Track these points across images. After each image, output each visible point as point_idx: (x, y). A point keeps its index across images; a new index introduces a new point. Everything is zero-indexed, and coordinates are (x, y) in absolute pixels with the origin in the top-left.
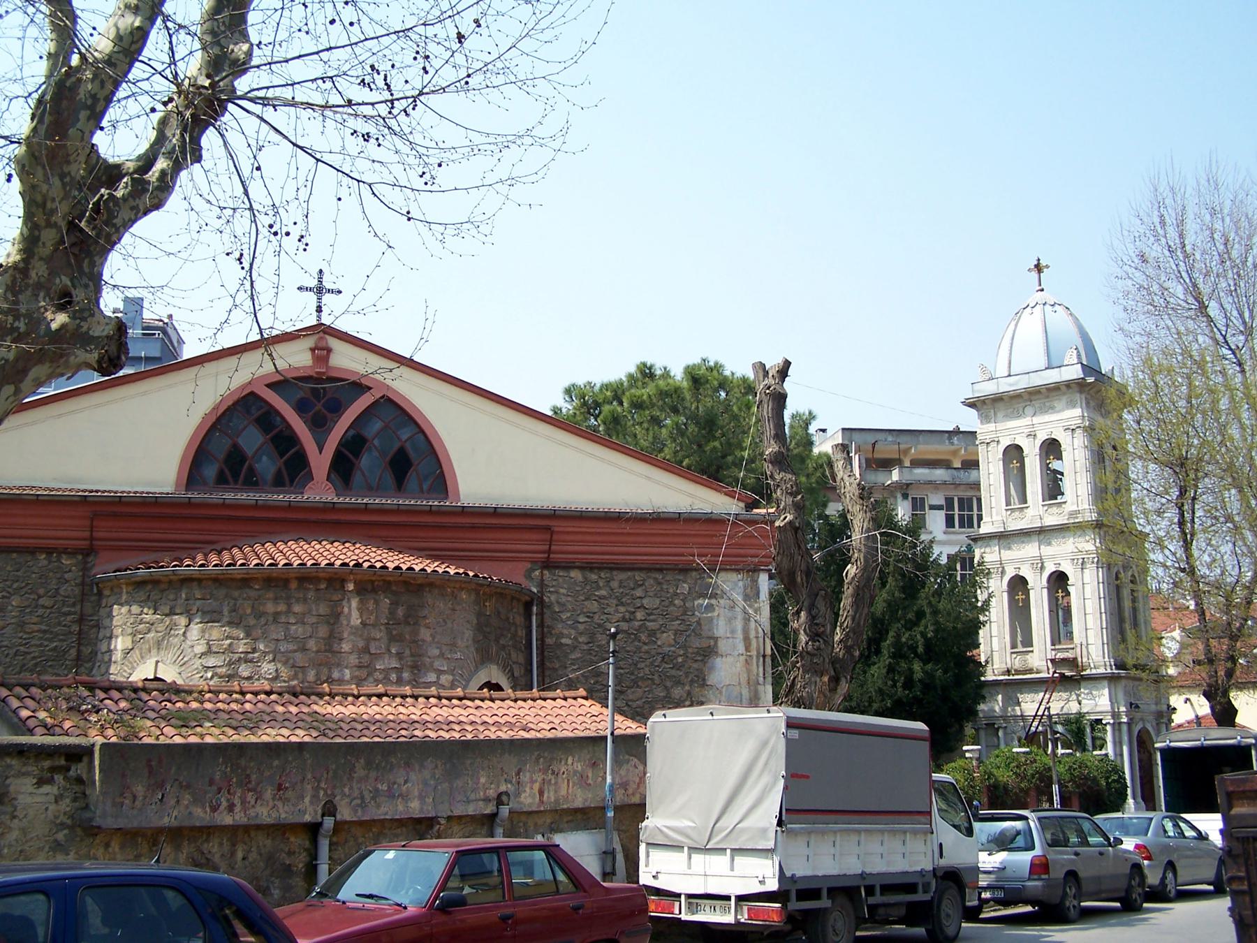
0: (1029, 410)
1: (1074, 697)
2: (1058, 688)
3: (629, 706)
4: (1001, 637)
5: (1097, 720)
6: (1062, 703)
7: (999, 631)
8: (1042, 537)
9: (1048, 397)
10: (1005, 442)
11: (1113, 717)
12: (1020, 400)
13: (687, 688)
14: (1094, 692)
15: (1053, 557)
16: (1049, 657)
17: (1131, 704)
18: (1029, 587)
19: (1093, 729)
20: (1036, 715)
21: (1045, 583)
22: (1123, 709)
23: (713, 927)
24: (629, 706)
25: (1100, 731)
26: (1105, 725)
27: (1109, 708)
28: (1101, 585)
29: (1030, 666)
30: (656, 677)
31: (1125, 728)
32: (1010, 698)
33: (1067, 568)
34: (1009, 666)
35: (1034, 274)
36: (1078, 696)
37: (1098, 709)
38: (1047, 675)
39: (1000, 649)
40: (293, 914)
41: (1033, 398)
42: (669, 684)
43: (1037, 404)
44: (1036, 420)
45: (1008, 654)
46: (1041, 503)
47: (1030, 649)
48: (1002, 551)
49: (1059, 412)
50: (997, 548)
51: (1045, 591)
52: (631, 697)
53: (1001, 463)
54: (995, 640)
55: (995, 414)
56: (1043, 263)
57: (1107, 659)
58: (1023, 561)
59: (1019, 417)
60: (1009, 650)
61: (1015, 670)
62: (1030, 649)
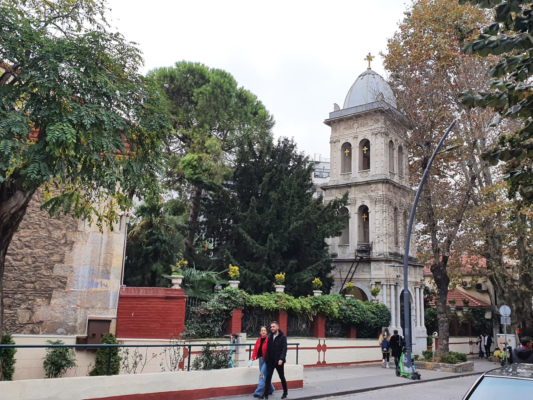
0: (356, 125)
3: (20, 240)
10: (343, 142)
12: (351, 121)
13: (64, 232)
18: (352, 147)
24: (20, 240)
30: (42, 223)
33: (367, 203)
35: (367, 62)
40: (316, 293)
42: (51, 228)
43: (360, 122)
52: (22, 234)
55: (340, 128)
56: (372, 55)
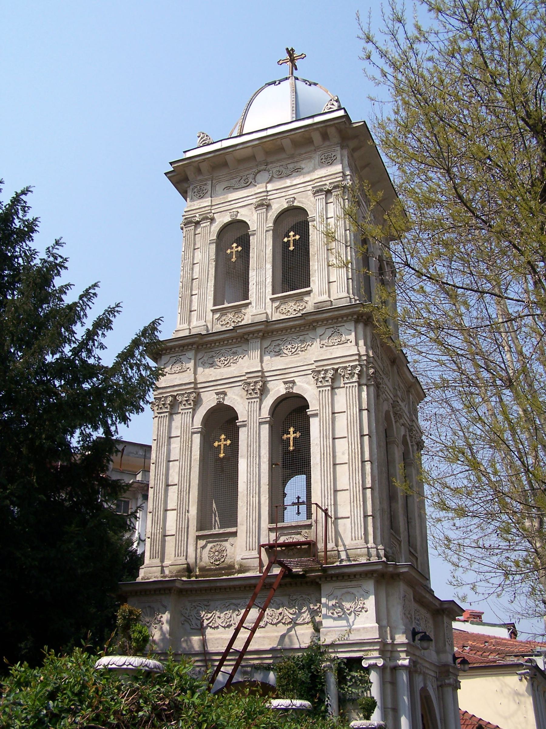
1: (306, 616)
2: (277, 599)
4: (181, 510)
5: (349, 659)
6: (282, 629)
7: (180, 499)
8: (266, 343)
9: (292, 156)
10: (223, 219)
11: (383, 653)
14: (347, 605)
15: (284, 371)
16: (264, 541)
17: (414, 633)
19: (341, 680)
20: (227, 652)
21: (265, 413)
22: (401, 638)
23: (151, 356)
25: (355, 685)
26: (367, 670)
27: (375, 635)
28: (365, 413)
29: (228, 561)
31: (404, 677)
32: (187, 620)
34: (191, 560)
36: (314, 613)
37: (354, 637)
38: (258, 574)
39: (179, 530)
41: (269, 160)
44: (270, 187)
45: (191, 540)
46: (269, 296)
47: (233, 530)
48: (200, 370)
49: (309, 173)
50: (191, 365)
51: (265, 429)
53: (213, 246)
54: (172, 516)
57: (371, 544)
58: (231, 382)
59: (247, 186)
60: (193, 532)
61: (202, 569)
62: (233, 530)
